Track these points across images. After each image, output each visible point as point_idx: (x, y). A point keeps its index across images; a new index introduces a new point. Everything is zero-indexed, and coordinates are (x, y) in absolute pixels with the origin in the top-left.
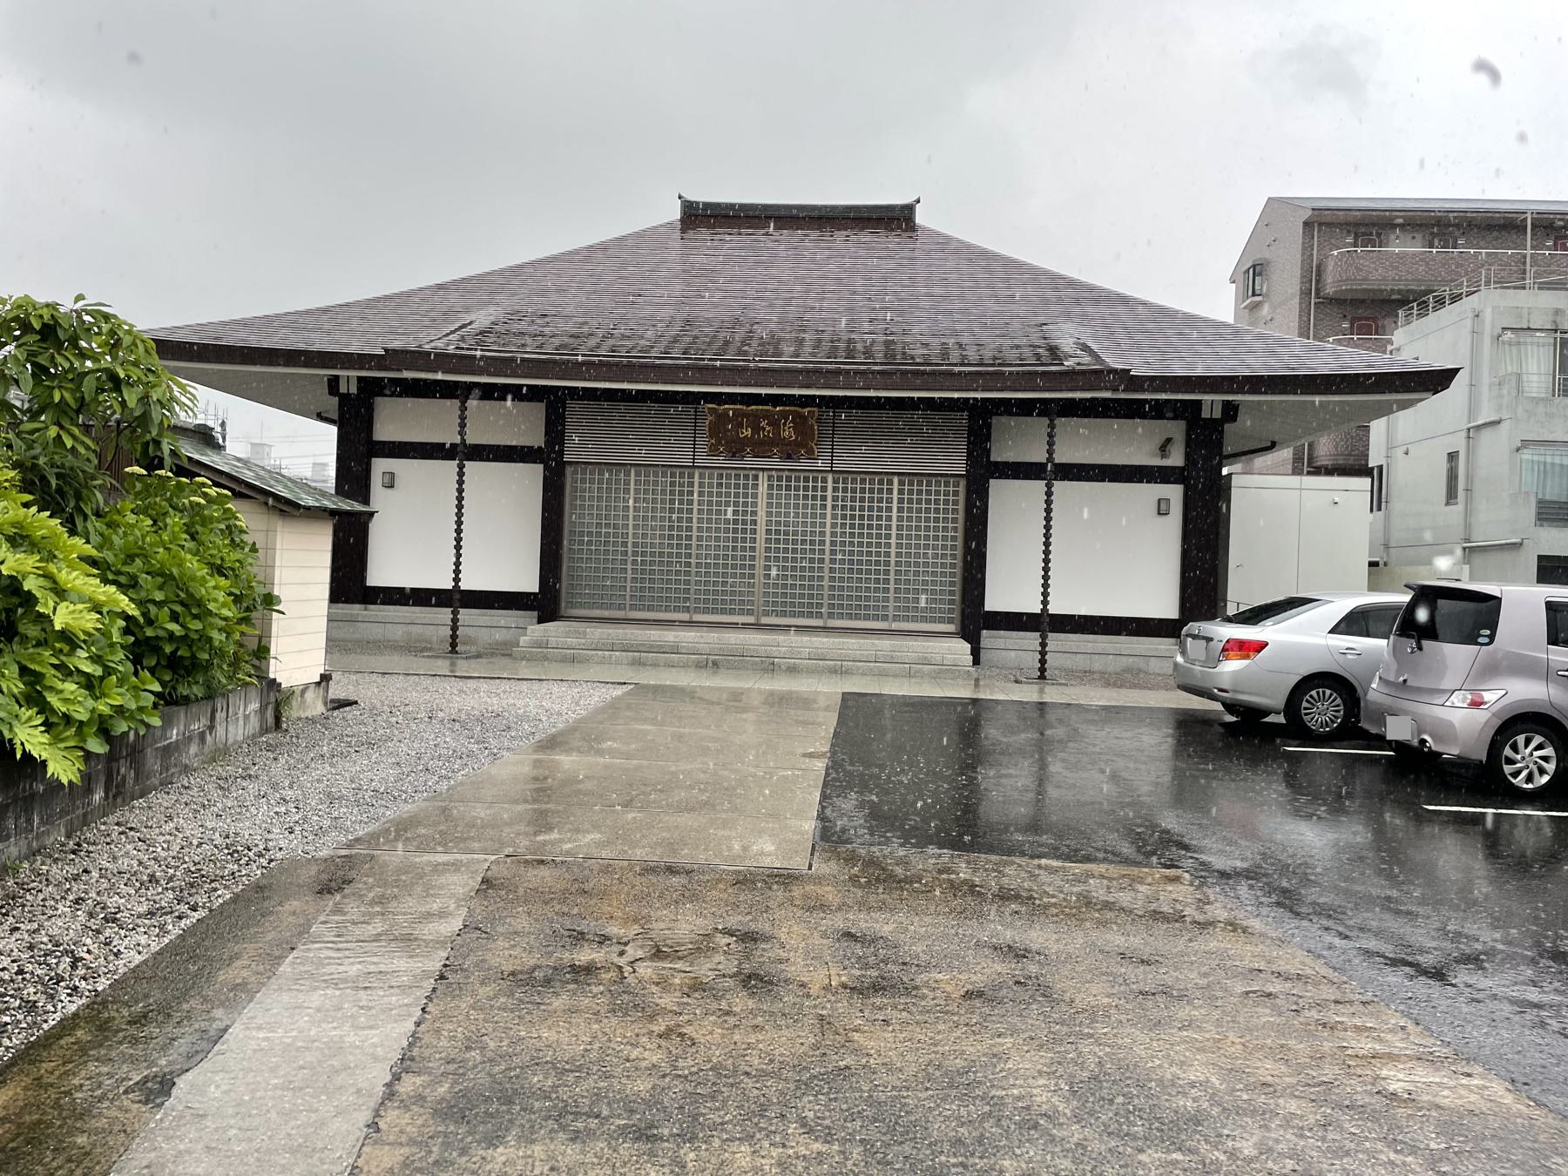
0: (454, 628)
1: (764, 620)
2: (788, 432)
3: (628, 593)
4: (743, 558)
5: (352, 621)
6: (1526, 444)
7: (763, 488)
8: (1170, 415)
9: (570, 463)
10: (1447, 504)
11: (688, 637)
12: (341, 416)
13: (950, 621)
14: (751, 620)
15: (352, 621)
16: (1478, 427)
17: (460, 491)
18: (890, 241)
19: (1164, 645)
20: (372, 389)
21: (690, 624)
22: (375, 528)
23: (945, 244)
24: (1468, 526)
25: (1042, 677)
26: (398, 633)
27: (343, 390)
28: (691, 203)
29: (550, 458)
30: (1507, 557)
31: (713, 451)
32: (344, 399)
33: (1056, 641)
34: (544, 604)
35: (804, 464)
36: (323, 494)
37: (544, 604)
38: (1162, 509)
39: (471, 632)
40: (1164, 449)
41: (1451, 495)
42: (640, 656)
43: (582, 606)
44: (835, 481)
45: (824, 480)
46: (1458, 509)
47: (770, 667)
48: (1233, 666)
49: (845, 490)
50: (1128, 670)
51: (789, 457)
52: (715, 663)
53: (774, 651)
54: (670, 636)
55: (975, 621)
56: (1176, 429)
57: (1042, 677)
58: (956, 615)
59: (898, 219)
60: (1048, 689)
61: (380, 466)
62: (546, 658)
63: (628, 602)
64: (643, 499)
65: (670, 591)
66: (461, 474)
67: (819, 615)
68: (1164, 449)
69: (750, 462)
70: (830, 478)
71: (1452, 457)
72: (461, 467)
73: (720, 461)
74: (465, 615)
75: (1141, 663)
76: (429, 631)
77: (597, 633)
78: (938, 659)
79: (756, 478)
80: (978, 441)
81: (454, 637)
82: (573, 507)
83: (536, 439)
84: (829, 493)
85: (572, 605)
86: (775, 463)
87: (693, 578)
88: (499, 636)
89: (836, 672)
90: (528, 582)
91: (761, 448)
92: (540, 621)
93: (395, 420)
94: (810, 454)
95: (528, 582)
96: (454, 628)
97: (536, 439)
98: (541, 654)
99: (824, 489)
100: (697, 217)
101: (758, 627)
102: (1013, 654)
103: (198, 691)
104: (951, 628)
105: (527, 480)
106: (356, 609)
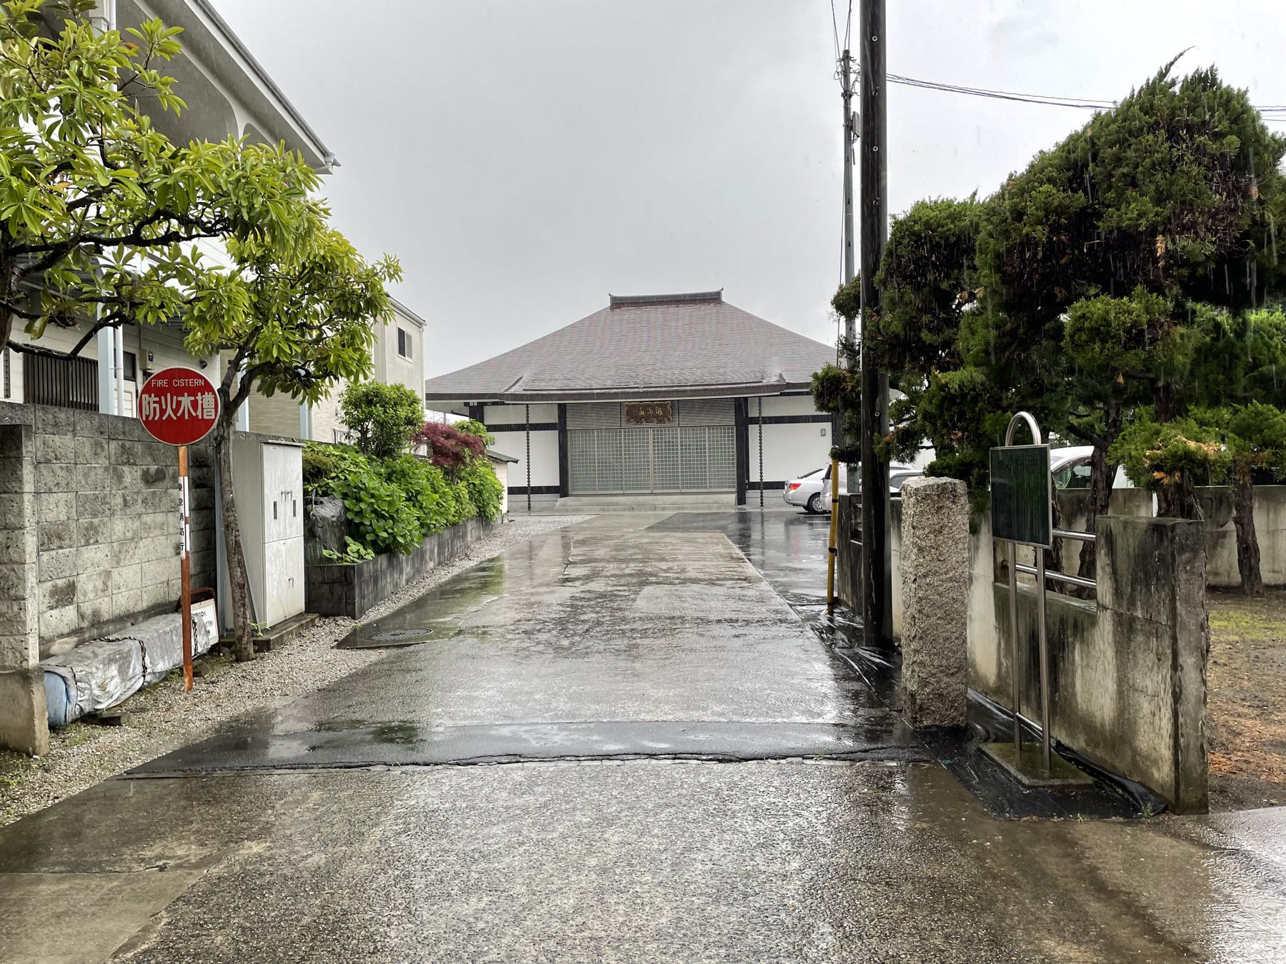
2: (660, 412)
7: (651, 432)
18: (709, 309)
20: (482, 405)
21: (624, 495)
22: (992, 579)
29: (560, 427)
31: (628, 421)
34: (561, 490)
35: (667, 424)
48: (792, 492)
65: (616, 481)
69: (645, 425)
73: (632, 425)
83: (554, 419)
86: (655, 425)
91: (648, 419)
97: (554, 419)
100: (618, 303)
101: (652, 494)
103: (89, 654)
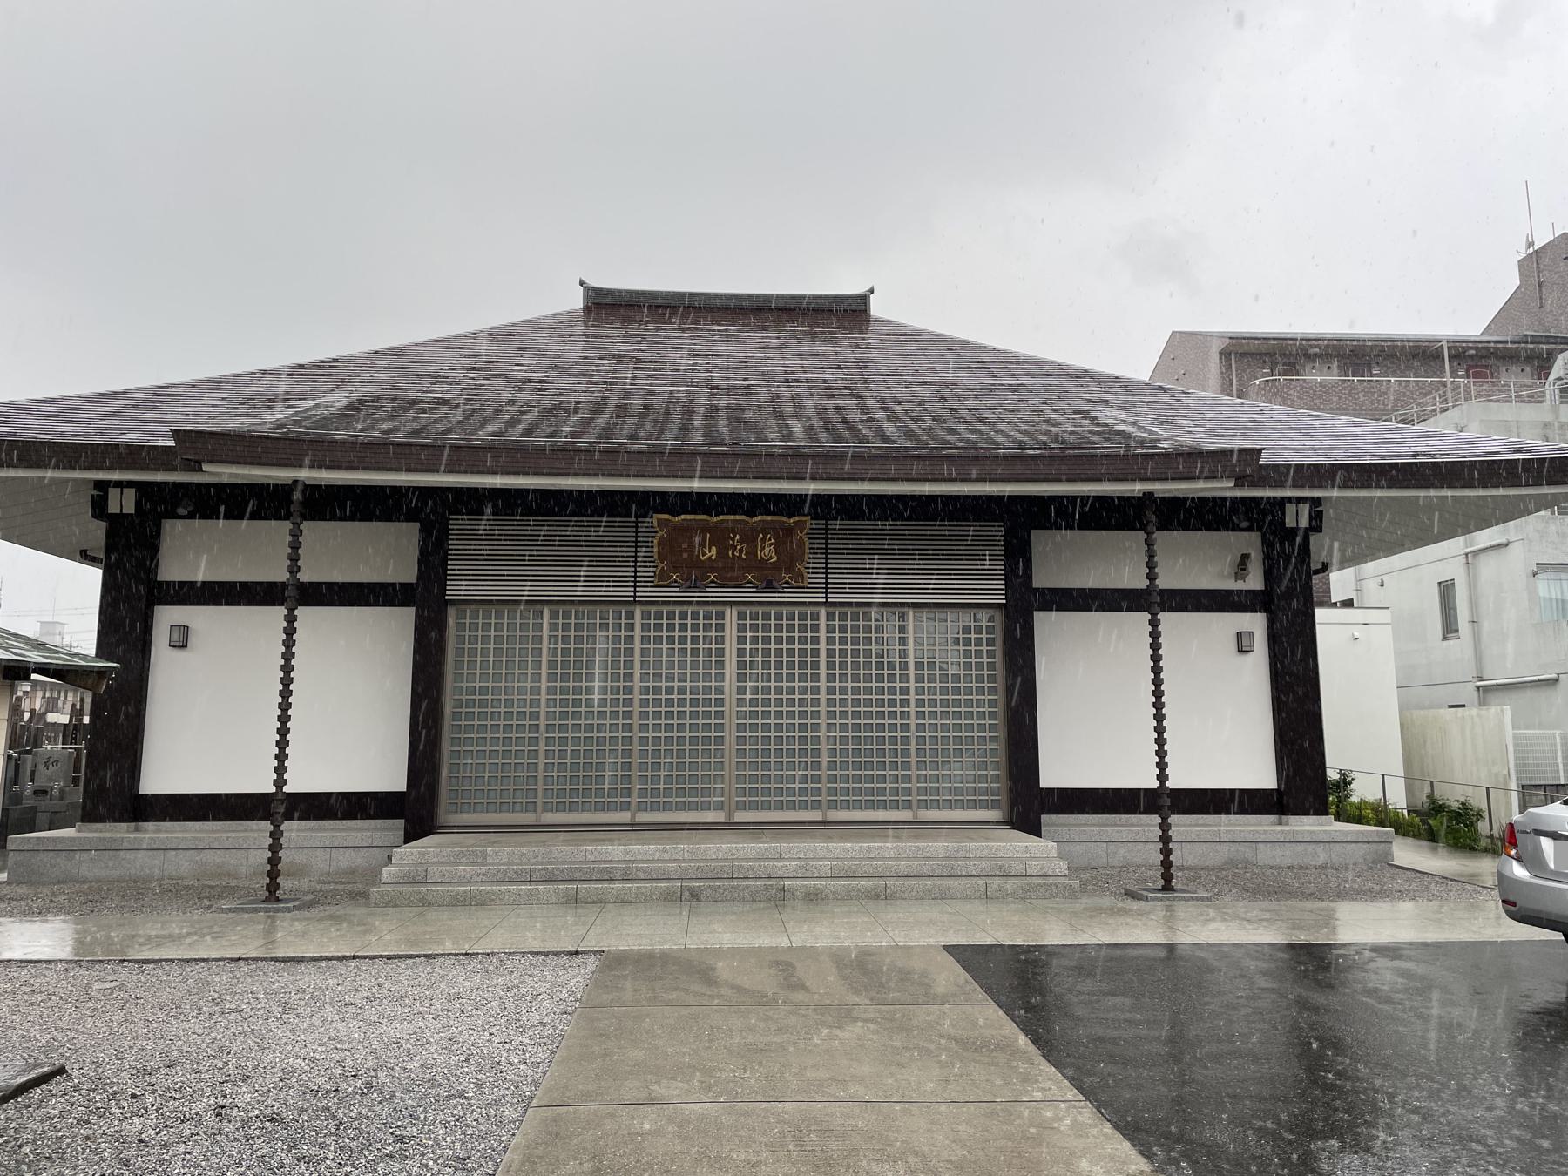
0: (275, 848)
1: (740, 816)
2: (768, 552)
3: (540, 787)
4: (707, 727)
5: (112, 848)
6: (1543, 567)
8: (1245, 524)
9: (453, 602)
10: (1445, 638)
11: (643, 851)
12: (109, 549)
13: (994, 805)
14: (720, 816)
15: (112, 848)
16: (1476, 553)
17: (287, 669)
19: (1262, 826)
20: (162, 503)
23: (904, 336)
24: (1479, 658)
25: (1167, 887)
26: (182, 865)
27: (113, 508)
28: (594, 289)
29: (425, 600)
30: (1541, 696)
31: (662, 580)
32: (117, 525)
33: (1183, 826)
34: (413, 809)
36: (85, 657)
37: (413, 809)
38: (1243, 645)
39: (300, 857)
40: (1242, 567)
41: (1449, 628)
42: (581, 891)
43: (472, 808)
44: (830, 616)
45: (815, 616)
46: (1460, 647)
47: (776, 896)
49: (843, 629)
50: (1231, 864)
51: (769, 586)
52: (695, 896)
53: (778, 867)
54: (616, 851)
55: (1029, 804)
56: (1250, 543)
57: (1167, 887)
58: (1003, 797)
59: (849, 313)
60: (1184, 909)
61: (167, 617)
62: (426, 903)
63: (540, 800)
64: (552, 653)
66: (290, 632)
67: (817, 805)
68: (1242, 567)
69: (715, 594)
70: (823, 612)
71: (1446, 589)
72: (290, 619)
73: (673, 594)
74: (294, 830)
75: (1247, 852)
76: (231, 859)
77: (505, 852)
78: (1017, 866)
79: (721, 615)
80: (1017, 555)
81: (274, 861)
82: (459, 665)
83: (404, 571)
84: (823, 635)
85: (458, 809)
86: (747, 594)
87: (636, 760)
88: (346, 860)
89: (877, 897)
90: (390, 776)
92: (409, 838)
93: (190, 552)
94: (799, 581)
95: (390, 776)
96: (275, 848)
98: (418, 897)
99: (815, 628)
100: (607, 307)
102: (1078, 847)
104: (993, 815)
105: (387, 637)
106: (121, 831)
